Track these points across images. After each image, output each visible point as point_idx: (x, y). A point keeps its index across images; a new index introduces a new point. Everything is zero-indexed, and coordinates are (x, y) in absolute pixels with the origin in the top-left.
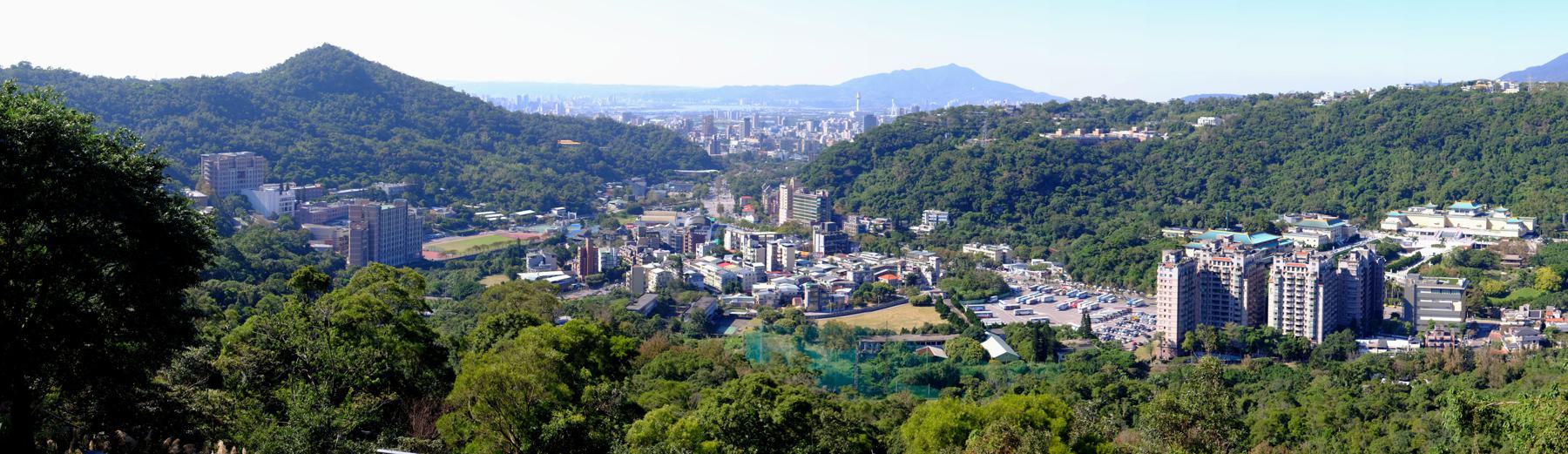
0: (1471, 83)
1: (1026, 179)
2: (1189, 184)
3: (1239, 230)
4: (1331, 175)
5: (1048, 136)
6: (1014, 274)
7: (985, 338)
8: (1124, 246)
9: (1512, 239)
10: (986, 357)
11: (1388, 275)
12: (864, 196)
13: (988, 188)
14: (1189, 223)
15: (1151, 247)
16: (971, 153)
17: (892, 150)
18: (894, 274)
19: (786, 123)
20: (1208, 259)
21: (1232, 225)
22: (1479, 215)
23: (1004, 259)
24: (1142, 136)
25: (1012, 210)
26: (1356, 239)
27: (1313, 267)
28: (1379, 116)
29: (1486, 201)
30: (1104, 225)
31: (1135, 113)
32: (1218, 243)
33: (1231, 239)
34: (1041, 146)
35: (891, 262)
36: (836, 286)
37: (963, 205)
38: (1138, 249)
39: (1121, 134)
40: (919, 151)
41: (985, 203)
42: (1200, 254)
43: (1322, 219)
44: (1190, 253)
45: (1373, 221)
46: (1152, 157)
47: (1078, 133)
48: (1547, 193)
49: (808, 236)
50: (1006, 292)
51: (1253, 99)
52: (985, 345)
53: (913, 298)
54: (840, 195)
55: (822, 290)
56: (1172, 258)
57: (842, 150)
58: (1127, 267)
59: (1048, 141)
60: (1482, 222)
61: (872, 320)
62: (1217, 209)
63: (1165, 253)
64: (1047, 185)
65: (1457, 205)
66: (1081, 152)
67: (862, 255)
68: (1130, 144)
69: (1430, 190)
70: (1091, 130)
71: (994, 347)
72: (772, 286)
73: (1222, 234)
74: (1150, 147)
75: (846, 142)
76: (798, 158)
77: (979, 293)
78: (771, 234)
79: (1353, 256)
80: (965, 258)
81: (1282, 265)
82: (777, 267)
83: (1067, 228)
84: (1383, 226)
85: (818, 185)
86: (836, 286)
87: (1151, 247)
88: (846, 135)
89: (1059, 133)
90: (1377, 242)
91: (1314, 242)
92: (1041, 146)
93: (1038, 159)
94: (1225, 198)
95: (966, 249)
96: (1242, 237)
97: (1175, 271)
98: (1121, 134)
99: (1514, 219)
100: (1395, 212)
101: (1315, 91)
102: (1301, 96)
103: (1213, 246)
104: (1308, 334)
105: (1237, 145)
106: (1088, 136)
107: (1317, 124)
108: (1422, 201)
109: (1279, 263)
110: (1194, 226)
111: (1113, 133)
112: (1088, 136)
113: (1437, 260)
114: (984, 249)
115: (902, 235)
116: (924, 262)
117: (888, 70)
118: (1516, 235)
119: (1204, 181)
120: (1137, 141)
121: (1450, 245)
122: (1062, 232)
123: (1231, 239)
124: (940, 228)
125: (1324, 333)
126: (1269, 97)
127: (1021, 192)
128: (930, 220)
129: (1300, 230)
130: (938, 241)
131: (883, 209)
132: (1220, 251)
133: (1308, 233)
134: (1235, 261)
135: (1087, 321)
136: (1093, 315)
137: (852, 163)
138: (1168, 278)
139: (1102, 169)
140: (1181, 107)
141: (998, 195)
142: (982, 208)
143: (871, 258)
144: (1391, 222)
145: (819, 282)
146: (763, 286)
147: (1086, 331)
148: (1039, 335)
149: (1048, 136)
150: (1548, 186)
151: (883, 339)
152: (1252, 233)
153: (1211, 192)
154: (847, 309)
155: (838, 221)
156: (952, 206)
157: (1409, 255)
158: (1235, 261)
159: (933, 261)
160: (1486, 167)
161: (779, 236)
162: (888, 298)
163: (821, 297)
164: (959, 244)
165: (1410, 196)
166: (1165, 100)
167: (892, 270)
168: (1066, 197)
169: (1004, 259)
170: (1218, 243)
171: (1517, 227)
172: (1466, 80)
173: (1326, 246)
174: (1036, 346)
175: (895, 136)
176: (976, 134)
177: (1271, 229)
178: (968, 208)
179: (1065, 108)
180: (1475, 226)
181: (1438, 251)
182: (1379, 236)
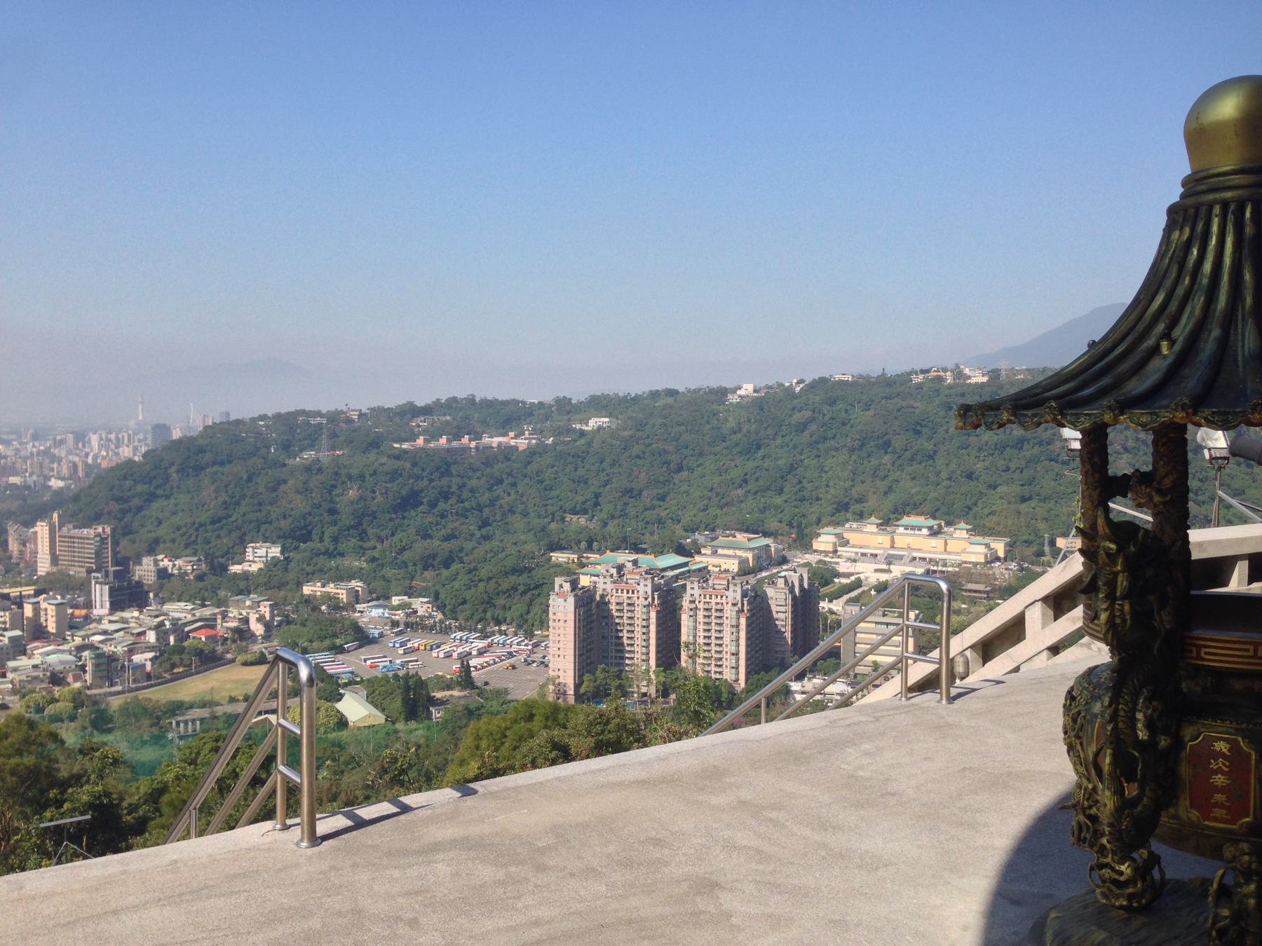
0: (923, 372)
1: (379, 499)
2: (580, 499)
3: (643, 551)
4: (752, 486)
5: (405, 446)
6: (371, 615)
7: (340, 697)
8: (506, 574)
9: (975, 564)
10: (342, 723)
11: (824, 605)
12: (161, 532)
13: (333, 512)
14: (583, 545)
15: (538, 574)
16: (308, 469)
17: (199, 469)
18: (213, 627)
19: (35, 437)
20: (609, 586)
21: (637, 549)
22: (935, 533)
23: (356, 597)
24: (522, 443)
25: (363, 536)
26: (784, 561)
27: (735, 594)
28: (808, 414)
29: (945, 513)
30: (480, 551)
31: (508, 415)
32: (620, 568)
33: (635, 562)
34: (397, 457)
35: (207, 612)
36: (131, 651)
37: (295, 536)
38: (523, 579)
39: (496, 441)
40: (238, 468)
41: (330, 531)
42: (598, 575)
43: (741, 537)
44: (585, 581)
45: (804, 542)
46: (532, 468)
47: (443, 440)
48: (1024, 507)
49: (84, 587)
50: (364, 639)
51: (655, 395)
52: (339, 706)
53: (240, 658)
54: (128, 531)
55: (112, 658)
56: (567, 586)
57: (126, 470)
58: (511, 601)
59: (406, 452)
60: (937, 543)
61: (193, 688)
62: (612, 528)
63: (558, 581)
64: (409, 502)
65: (906, 520)
66: (445, 464)
67: (167, 607)
68: (507, 453)
69: (872, 503)
70: (458, 437)
71: (355, 708)
72: (37, 660)
73: (624, 557)
74: (532, 453)
75: (130, 462)
76: (56, 484)
77: (327, 642)
78: (29, 590)
79: (781, 582)
80: (308, 600)
81: (697, 592)
82: (39, 633)
83: (434, 556)
84: (816, 545)
85: (96, 519)
86: (131, 651)
87: (538, 574)
88: (126, 452)
89: (420, 441)
90: (807, 565)
91: (733, 566)
92: (397, 457)
93: (394, 475)
94: (624, 515)
95: (307, 590)
96: (646, 560)
97: (571, 600)
98: (496, 441)
99: (979, 539)
100: (829, 529)
101: (728, 384)
102: (712, 392)
103: (614, 571)
104: (728, 675)
105: (636, 450)
106: (455, 444)
107: (732, 423)
108: (860, 516)
109: (693, 590)
110: (590, 548)
111: (486, 440)
112: (455, 444)
113: (881, 587)
114: (331, 588)
115: (214, 582)
116: (254, 613)
117: (502, 397)
118: (983, 560)
119: (597, 495)
120: (516, 448)
121: (897, 571)
122: (427, 563)
123: (635, 562)
124: (272, 564)
125: (748, 674)
126: (672, 393)
127: (374, 515)
128: (259, 556)
129: (715, 553)
130: (272, 581)
131: (189, 546)
132: (624, 581)
133: (725, 556)
134: (641, 588)
135: (466, 669)
136: (473, 662)
137: (140, 488)
138: (562, 609)
139: (473, 483)
140: (253, 420)
141: (346, 519)
142: (315, 536)
143: (179, 610)
144: (824, 541)
145: (107, 648)
146: (23, 662)
147: (465, 679)
148: (407, 689)
149: (405, 446)
150: (1024, 500)
151: (205, 713)
152: (659, 552)
153: (607, 508)
154: (150, 679)
155: (124, 564)
156: (284, 537)
157: (845, 581)
158: (641, 588)
159: (265, 609)
160: (944, 475)
161: (38, 593)
162: (209, 660)
163: (109, 667)
164: (299, 585)
165: (846, 509)
166: (548, 397)
167: (210, 623)
168: (430, 519)
169: (356, 597)
170: (620, 568)
171: (982, 549)
172: (918, 368)
173: (745, 571)
174: (406, 701)
175: (201, 450)
176: (311, 447)
177: (681, 550)
178: (306, 538)
179: (427, 411)
180: (931, 547)
181: (883, 577)
182: (812, 558)
